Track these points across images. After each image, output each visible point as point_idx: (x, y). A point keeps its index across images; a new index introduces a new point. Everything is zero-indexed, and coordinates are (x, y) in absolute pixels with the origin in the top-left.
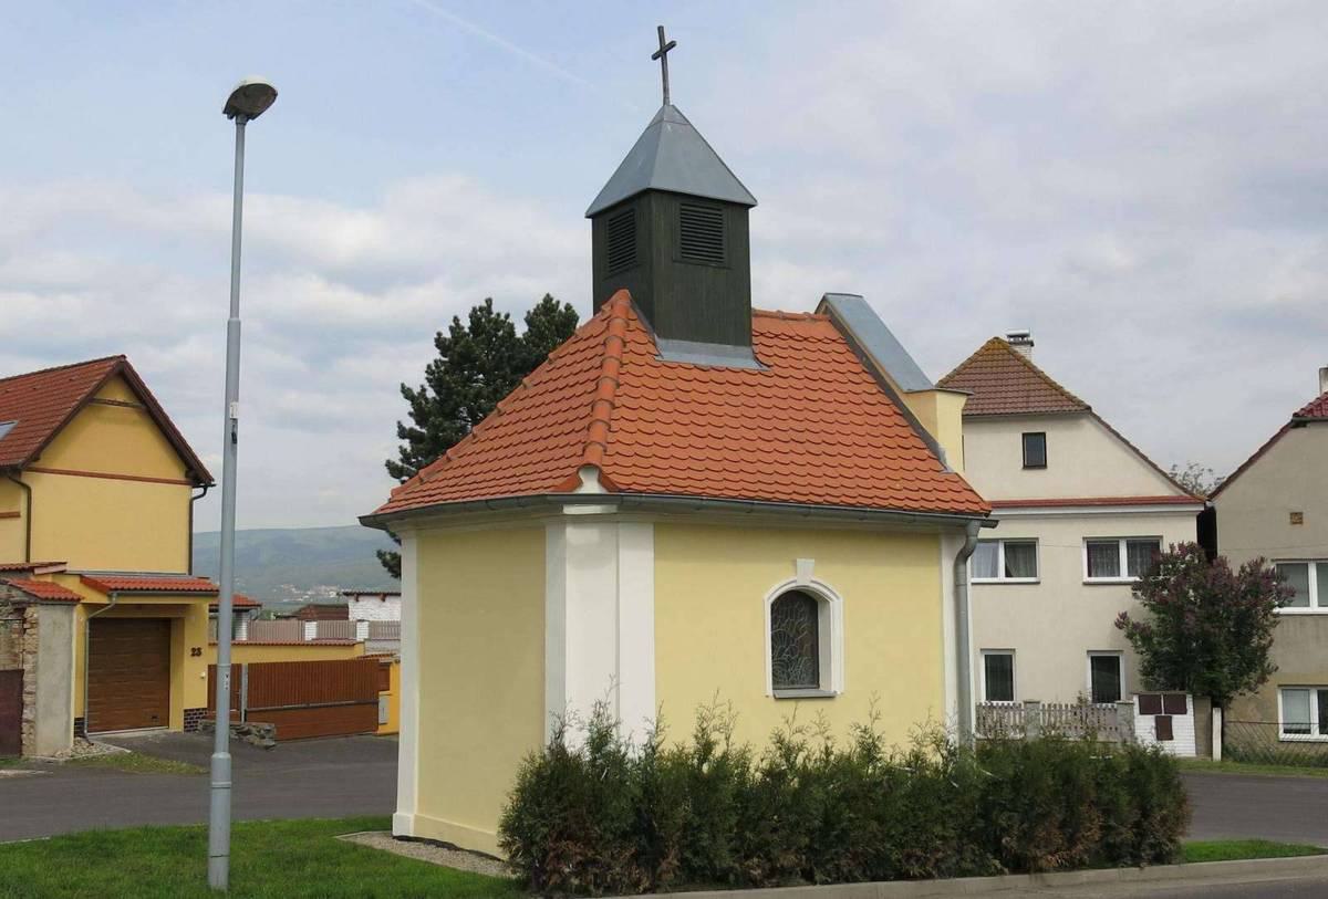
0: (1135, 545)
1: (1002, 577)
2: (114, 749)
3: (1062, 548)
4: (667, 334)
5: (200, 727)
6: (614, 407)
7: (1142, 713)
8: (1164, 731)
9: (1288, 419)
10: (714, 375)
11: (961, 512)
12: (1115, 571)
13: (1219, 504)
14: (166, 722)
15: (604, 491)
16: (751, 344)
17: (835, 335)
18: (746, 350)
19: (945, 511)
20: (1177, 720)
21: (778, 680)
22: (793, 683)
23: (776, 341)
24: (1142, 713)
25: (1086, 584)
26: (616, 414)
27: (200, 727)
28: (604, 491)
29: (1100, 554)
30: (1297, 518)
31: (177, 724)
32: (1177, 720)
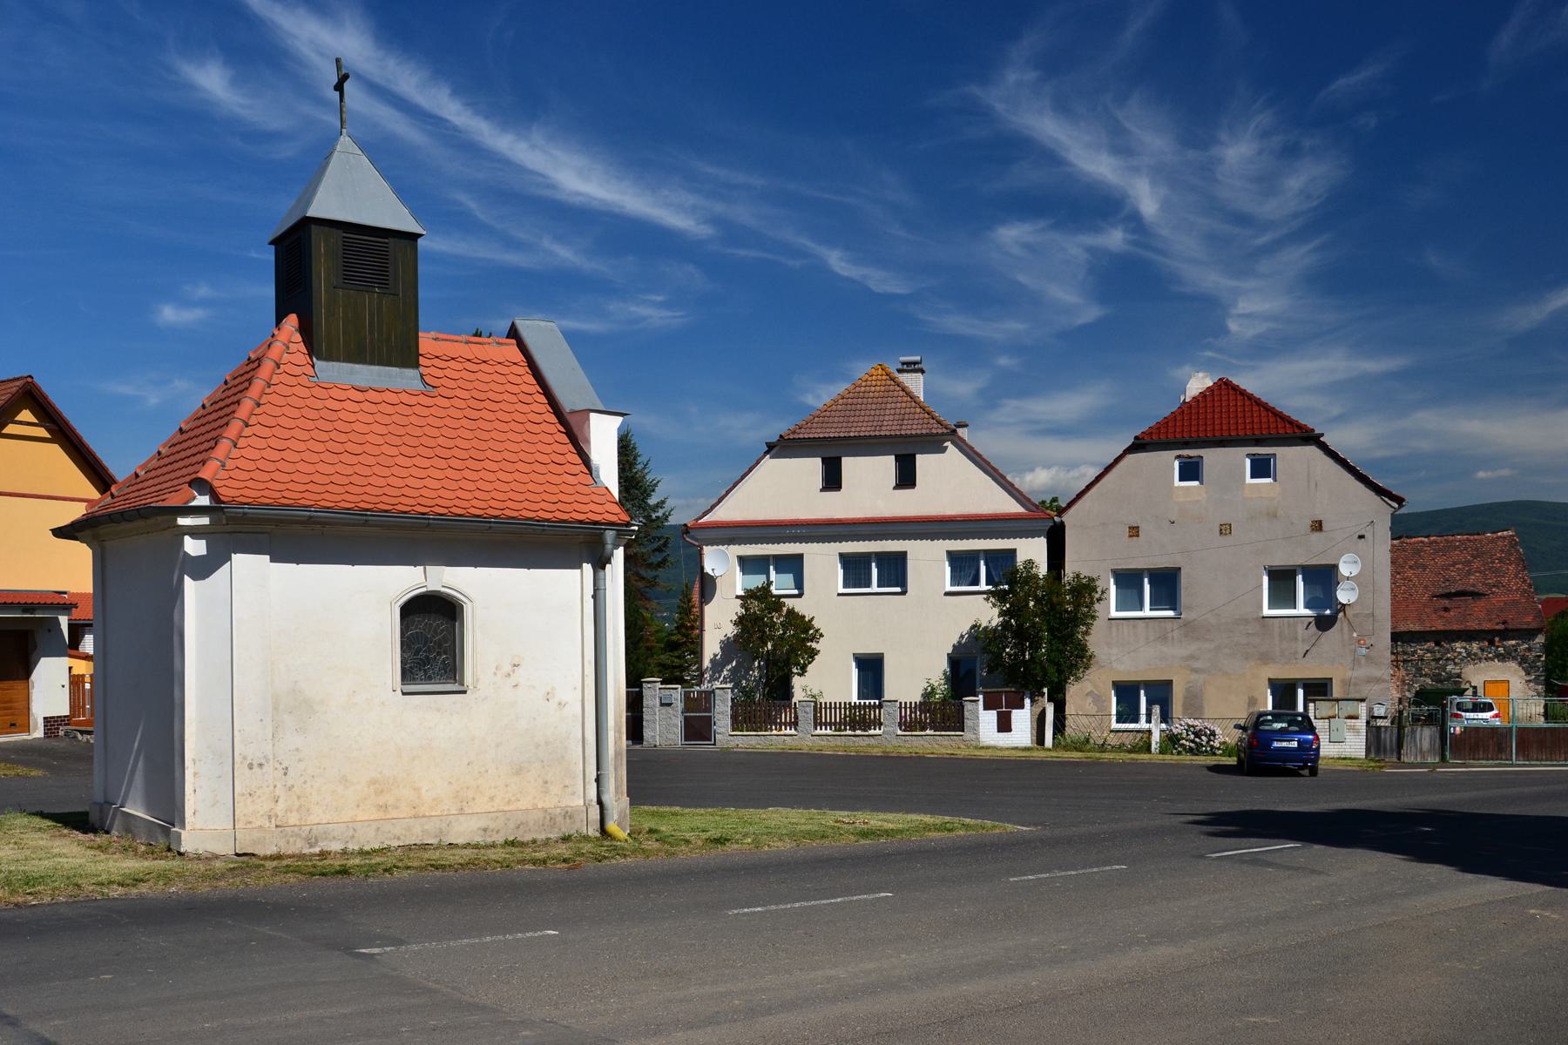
0: (992, 557)
1: (875, 588)
2: (140, 765)
3: (928, 561)
4: (329, 358)
5: (61, 733)
6: (247, 425)
7: (986, 708)
8: (1004, 725)
9: (1130, 441)
10: (372, 395)
11: (596, 523)
12: (976, 582)
13: (1067, 518)
14: (26, 728)
15: (1021, 510)
16: (416, 365)
17: (519, 357)
18: (411, 373)
19: (581, 522)
20: (1016, 713)
21: (407, 674)
22: (430, 678)
23: (484, 367)
24: (986, 708)
25: (947, 594)
26: (247, 432)
27: (61, 733)
28: (1021, 510)
29: (963, 566)
30: (1134, 531)
31: (39, 733)
32: (1016, 713)
